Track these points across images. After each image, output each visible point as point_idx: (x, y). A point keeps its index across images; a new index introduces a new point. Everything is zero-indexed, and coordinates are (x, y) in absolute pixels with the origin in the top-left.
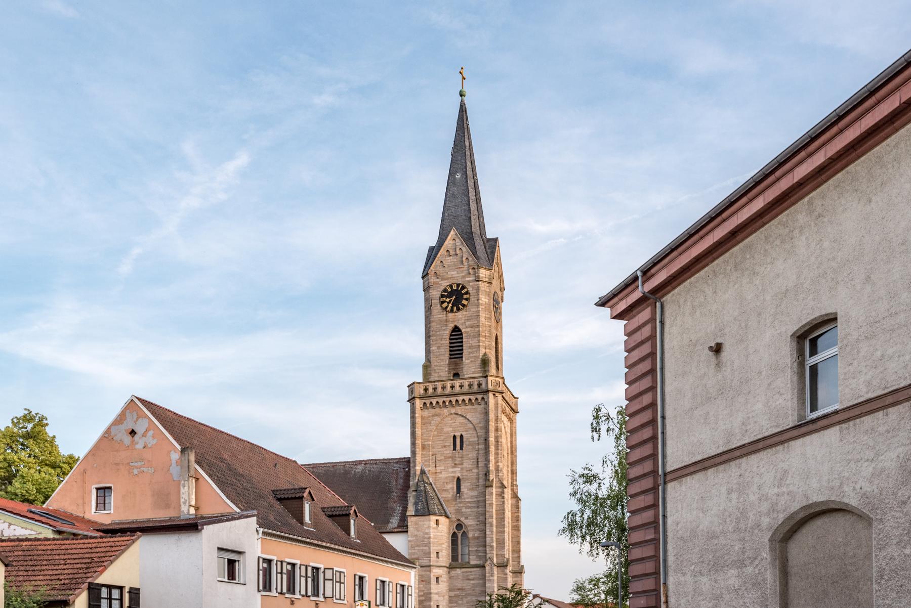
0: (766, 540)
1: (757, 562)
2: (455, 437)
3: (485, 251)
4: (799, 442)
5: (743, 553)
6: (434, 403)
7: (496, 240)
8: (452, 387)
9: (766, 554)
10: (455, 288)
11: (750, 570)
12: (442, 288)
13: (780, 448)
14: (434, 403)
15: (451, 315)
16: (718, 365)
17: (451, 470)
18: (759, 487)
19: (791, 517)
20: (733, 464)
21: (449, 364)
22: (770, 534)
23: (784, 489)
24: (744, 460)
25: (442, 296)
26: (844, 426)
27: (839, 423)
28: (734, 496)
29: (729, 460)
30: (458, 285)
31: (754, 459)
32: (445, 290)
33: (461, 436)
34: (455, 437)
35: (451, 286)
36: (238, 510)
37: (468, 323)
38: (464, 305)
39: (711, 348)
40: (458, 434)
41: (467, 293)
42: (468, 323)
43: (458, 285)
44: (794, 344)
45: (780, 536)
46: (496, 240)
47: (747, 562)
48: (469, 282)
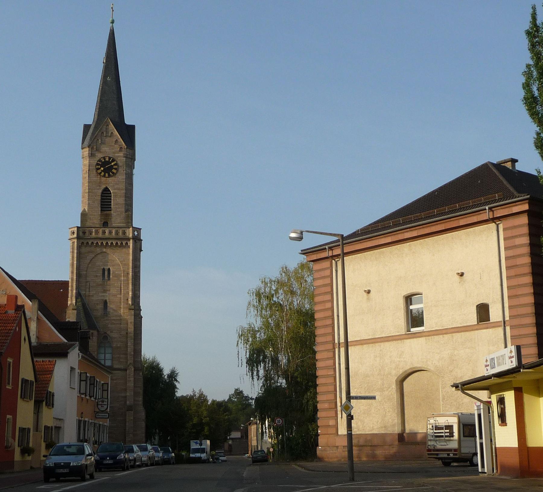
0: (394, 381)
1: (390, 389)
2: (104, 270)
3: (128, 133)
4: (408, 341)
5: (383, 385)
6: (90, 243)
7: (133, 127)
8: (104, 232)
9: (394, 386)
10: (107, 159)
11: (386, 393)
12: (98, 159)
13: (399, 341)
14: (90, 243)
15: (103, 179)
16: (368, 299)
17: (101, 294)
18: (390, 357)
19: (406, 371)
20: (377, 344)
21: (101, 215)
22: (396, 378)
23: (402, 359)
24: (382, 344)
25: (97, 164)
26: (428, 338)
27: (425, 336)
28: (378, 359)
29: (375, 342)
30: (110, 158)
31: (387, 344)
32: (100, 161)
33: (109, 270)
34: (104, 270)
35: (104, 158)
36: (66, 341)
37: (116, 186)
38: (113, 173)
39: (365, 291)
40: (106, 268)
41: (104, 158)
42: (116, 186)
43: (110, 158)
44: (404, 299)
45: (400, 378)
46: (133, 127)
47: (385, 389)
48: (119, 156)
